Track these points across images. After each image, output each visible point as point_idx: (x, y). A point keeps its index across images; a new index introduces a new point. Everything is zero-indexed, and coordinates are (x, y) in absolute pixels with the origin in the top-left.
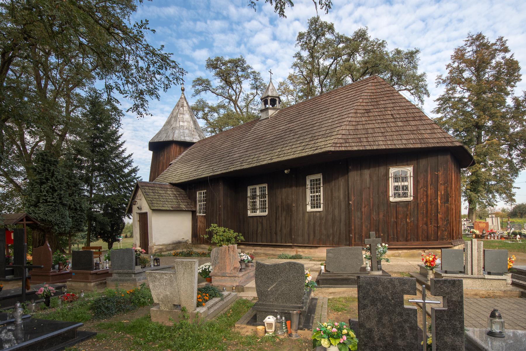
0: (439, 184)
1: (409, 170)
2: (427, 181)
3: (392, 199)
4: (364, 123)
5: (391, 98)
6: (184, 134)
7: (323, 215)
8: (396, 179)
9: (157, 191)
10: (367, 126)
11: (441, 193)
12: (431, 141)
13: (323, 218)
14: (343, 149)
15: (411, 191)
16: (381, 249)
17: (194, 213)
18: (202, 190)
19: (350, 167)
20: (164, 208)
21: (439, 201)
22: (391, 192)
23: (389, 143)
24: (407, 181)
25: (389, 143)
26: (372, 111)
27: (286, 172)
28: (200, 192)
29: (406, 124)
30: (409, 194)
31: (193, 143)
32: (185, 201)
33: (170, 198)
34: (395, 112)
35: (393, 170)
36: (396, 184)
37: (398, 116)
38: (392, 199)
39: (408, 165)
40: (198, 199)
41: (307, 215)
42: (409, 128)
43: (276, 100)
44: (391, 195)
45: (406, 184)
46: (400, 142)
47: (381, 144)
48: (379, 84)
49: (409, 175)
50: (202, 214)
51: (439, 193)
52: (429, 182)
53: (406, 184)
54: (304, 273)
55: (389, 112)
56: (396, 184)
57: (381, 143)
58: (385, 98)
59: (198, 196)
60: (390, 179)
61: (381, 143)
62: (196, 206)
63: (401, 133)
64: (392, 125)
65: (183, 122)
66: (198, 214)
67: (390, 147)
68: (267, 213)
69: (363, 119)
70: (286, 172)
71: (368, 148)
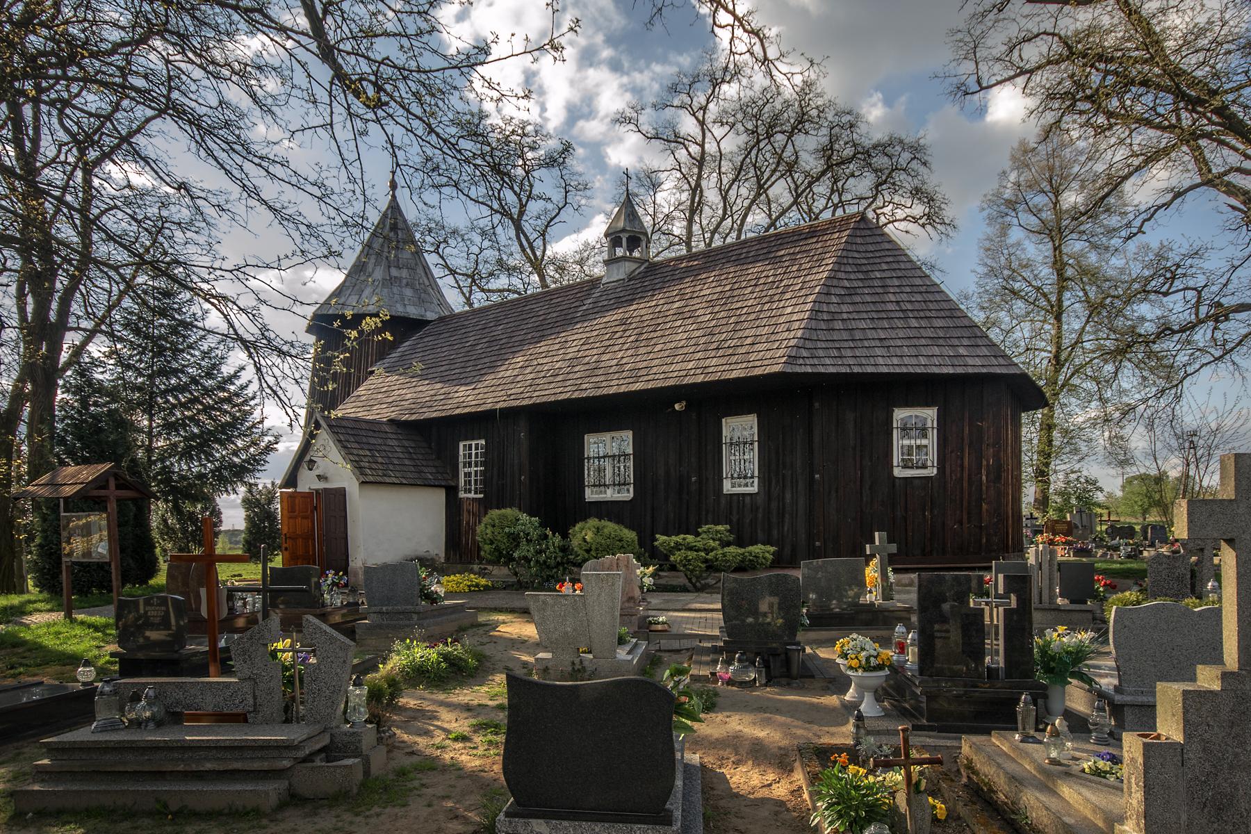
0: (984, 447)
1: (929, 415)
2: (963, 440)
3: (898, 472)
4: (845, 316)
5: (895, 266)
6: (403, 300)
7: (760, 500)
8: (905, 430)
9: (364, 440)
10: (854, 324)
11: (988, 461)
12: (970, 361)
13: (757, 508)
14: (809, 370)
15: (932, 456)
16: (495, 767)
17: (451, 491)
18: (473, 439)
19: (817, 405)
20: (387, 480)
21: (984, 478)
22: (896, 458)
23: (895, 361)
24: (925, 436)
25: (895, 361)
26: (859, 291)
27: (677, 407)
28: (467, 443)
29: (923, 323)
30: (929, 463)
31: (429, 322)
32: (430, 463)
33: (396, 455)
34: (904, 297)
35: (900, 414)
36: (906, 442)
37: (909, 307)
38: (898, 472)
39: (927, 405)
40: (461, 459)
41: (723, 501)
42: (930, 333)
43: (639, 239)
44: (895, 464)
45: (924, 442)
46: (914, 361)
47: (884, 364)
48: (869, 232)
49: (929, 425)
50: (472, 495)
51: (984, 463)
52: (966, 441)
53: (924, 442)
54: (509, 716)
55: (892, 298)
56: (906, 442)
57: (881, 360)
58: (885, 267)
59: (461, 453)
60: (895, 432)
61: (881, 360)
62: (456, 475)
63: (916, 342)
64: (900, 324)
65: (398, 267)
66: (462, 495)
67: (898, 370)
68: (631, 495)
69: (845, 308)
70: (677, 407)
71: (856, 370)
